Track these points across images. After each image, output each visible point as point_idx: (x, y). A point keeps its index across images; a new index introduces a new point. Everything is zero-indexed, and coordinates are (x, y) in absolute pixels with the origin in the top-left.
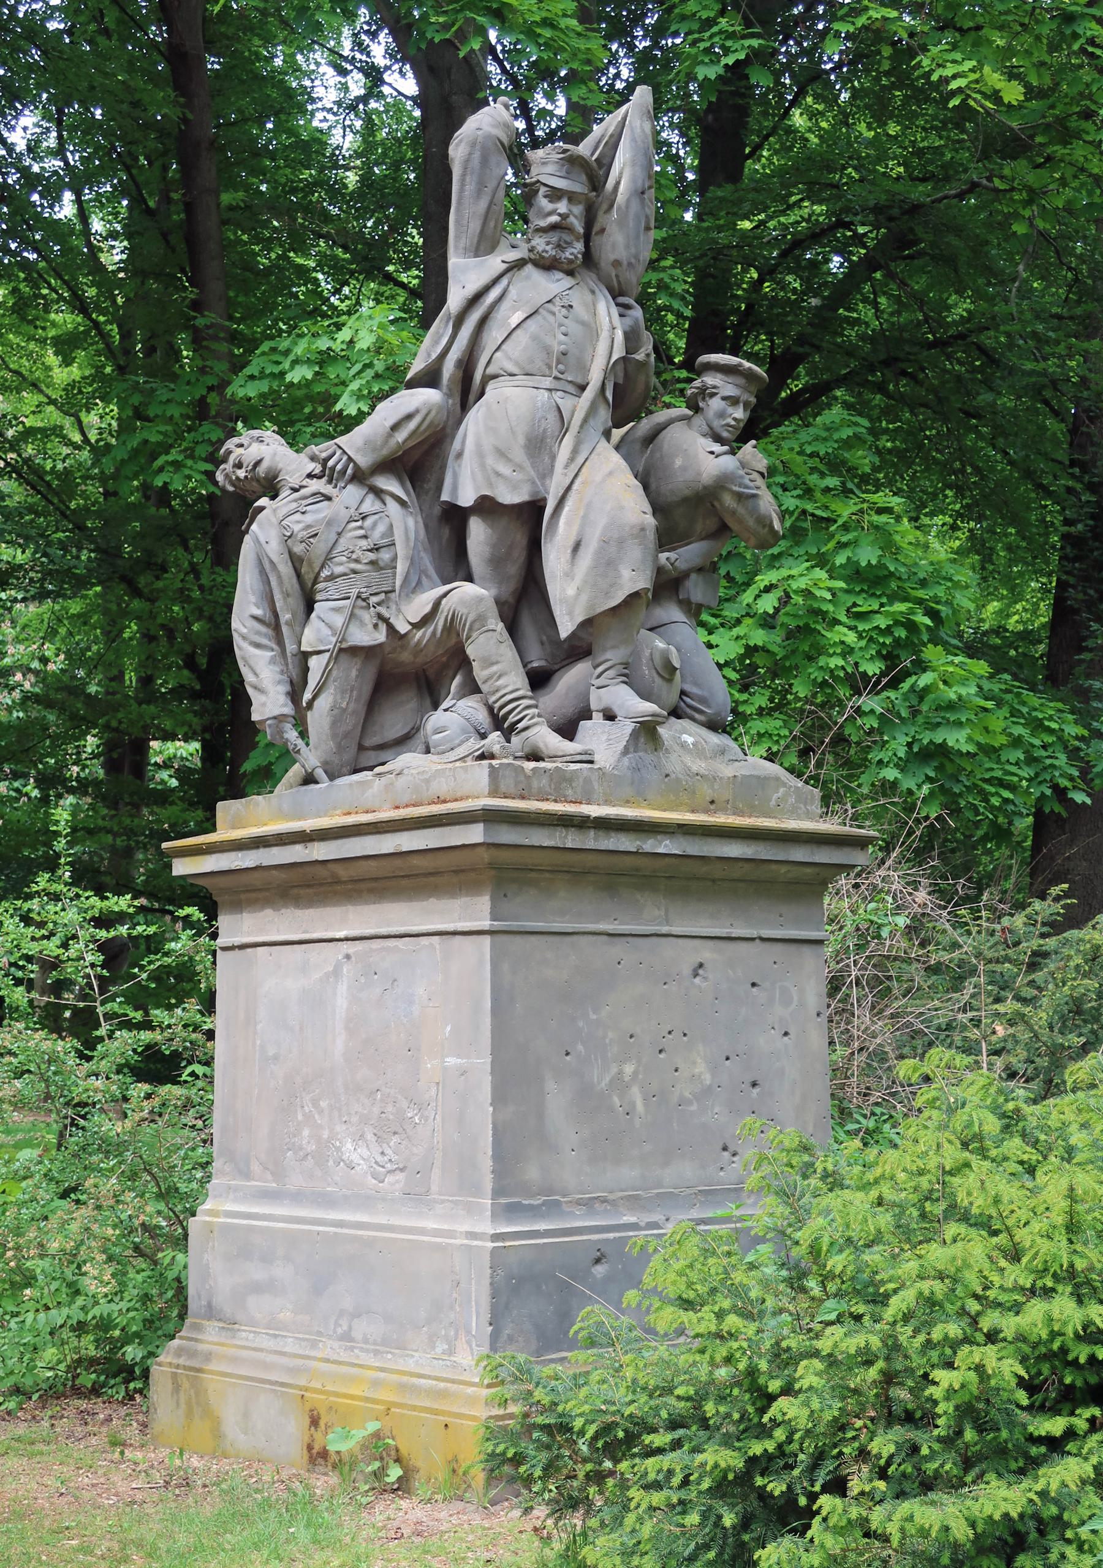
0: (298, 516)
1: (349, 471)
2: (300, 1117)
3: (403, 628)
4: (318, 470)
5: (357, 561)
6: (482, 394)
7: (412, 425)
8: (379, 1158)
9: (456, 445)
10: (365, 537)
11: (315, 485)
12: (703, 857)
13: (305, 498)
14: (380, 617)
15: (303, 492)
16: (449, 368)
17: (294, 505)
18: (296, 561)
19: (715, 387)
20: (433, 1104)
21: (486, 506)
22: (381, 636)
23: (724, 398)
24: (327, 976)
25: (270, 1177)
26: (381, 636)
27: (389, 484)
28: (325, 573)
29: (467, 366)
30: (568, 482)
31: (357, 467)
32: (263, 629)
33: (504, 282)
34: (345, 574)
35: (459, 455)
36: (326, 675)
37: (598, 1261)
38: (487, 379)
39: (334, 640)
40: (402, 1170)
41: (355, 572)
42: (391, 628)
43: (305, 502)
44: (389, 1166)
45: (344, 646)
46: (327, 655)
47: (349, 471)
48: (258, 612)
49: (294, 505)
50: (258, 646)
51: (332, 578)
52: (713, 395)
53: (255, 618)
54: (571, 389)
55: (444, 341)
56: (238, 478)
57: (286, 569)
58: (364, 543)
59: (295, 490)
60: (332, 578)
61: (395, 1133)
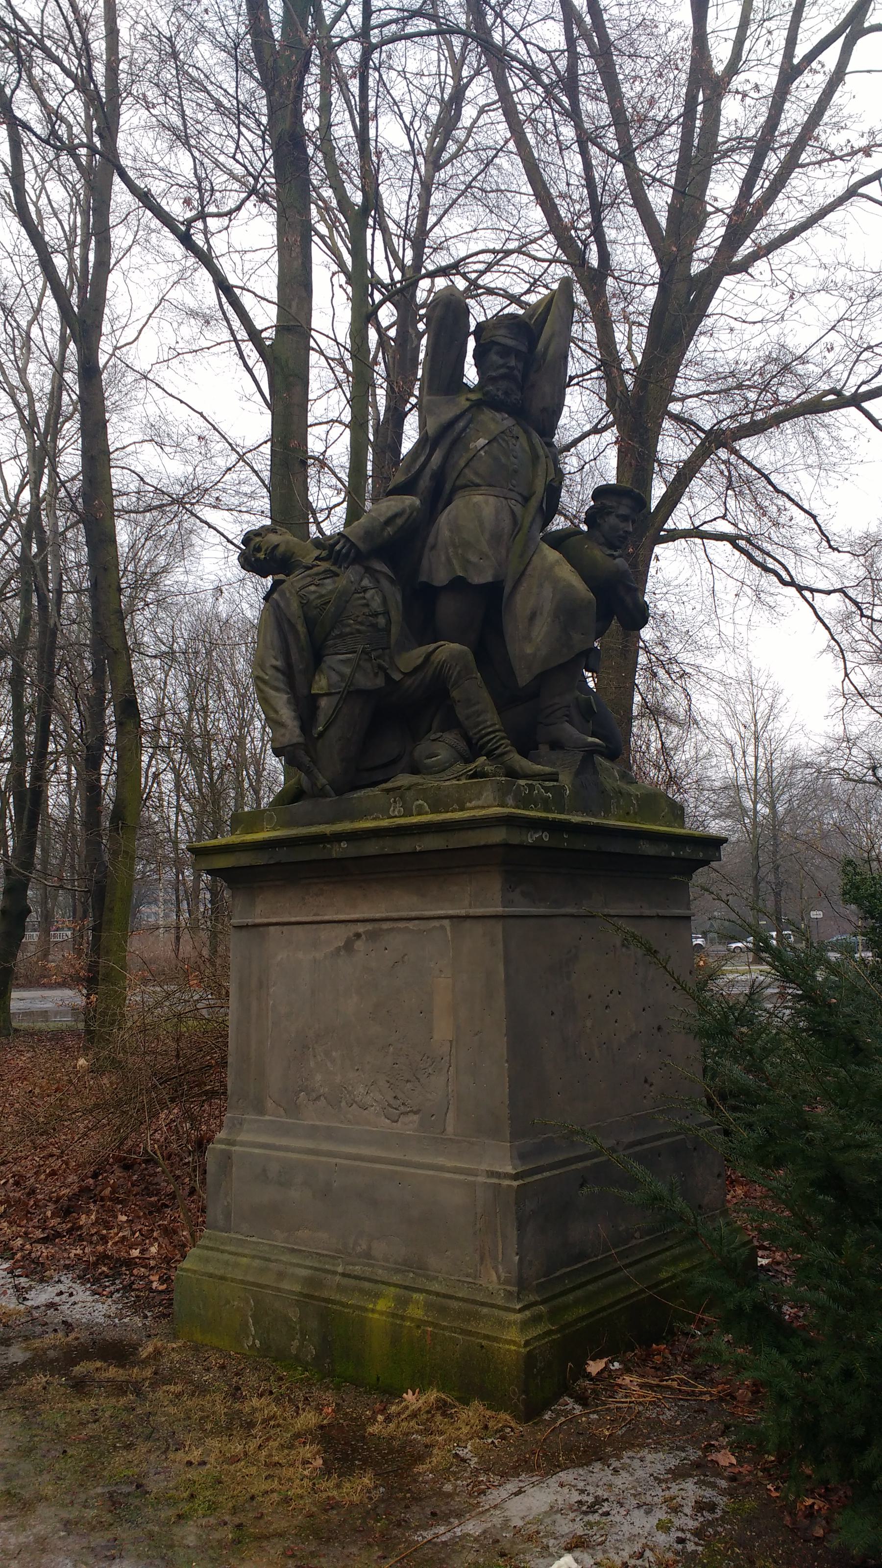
0: (313, 588)
1: (352, 555)
2: (312, 1064)
3: (397, 677)
4: (324, 554)
5: (361, 623)
6: (449, 502)
7: (400, 521)
8: (392, 1101)
9: (431, 540)
10: (367, 605)
11: (324, 565)
12: (324, 860)
13: (317, 574)
14: (380, 667)
15: (315, 570)
16: (425, 482)
17: (309, 579)
18: (309, 623)
19: (611, 507)
20: (447, 1058)
21: (458, 584)
22: (380, 682)
23: (618, 516)
24: (338, 949)
25: (282, 1112)
26: (380, 682)
27: (380, 566)
28: (337, 632)
29: (439, 477)
30: (522, 568)
31: (358, 550)
32: (280, 676)
33: (469, 416)
34: (352, 634)
35: (433, 547)
36: (337, 711)
37: (582, 1186)
38: (454, 490)
39: (344, 685)
40: (416, 1113)
41: (359, 631)
42: (388, 678)
43: (322, 577)
44: (402, 1108)
45: (352, 688)
46: (338, 697)
47: (352, 555)
48: (278, 663)
49: (309, 579)
50: (277, 689)
51: (341, 636)
52: (609, 513)
53: (275, 668)
54: (520, 499)
55: (422, 459)
56: (257, 560)
57: (301, 629)
58: (366, 610)
59: (308, 568)
60: (341, 636)
61: (408, 1081)
